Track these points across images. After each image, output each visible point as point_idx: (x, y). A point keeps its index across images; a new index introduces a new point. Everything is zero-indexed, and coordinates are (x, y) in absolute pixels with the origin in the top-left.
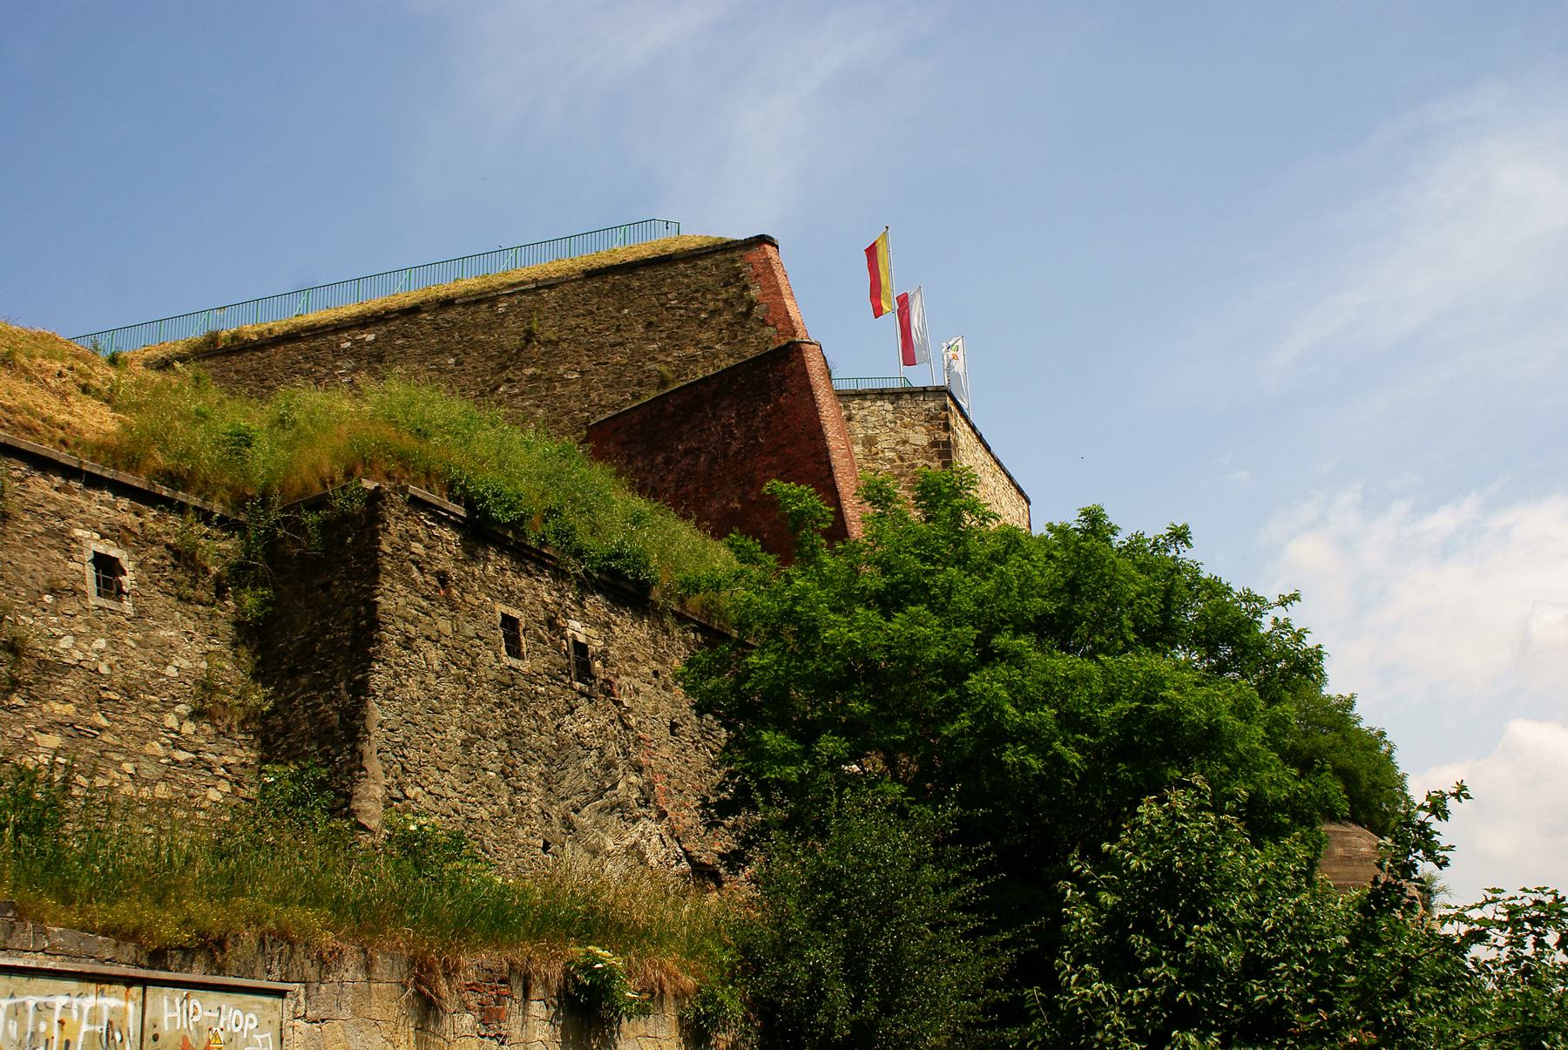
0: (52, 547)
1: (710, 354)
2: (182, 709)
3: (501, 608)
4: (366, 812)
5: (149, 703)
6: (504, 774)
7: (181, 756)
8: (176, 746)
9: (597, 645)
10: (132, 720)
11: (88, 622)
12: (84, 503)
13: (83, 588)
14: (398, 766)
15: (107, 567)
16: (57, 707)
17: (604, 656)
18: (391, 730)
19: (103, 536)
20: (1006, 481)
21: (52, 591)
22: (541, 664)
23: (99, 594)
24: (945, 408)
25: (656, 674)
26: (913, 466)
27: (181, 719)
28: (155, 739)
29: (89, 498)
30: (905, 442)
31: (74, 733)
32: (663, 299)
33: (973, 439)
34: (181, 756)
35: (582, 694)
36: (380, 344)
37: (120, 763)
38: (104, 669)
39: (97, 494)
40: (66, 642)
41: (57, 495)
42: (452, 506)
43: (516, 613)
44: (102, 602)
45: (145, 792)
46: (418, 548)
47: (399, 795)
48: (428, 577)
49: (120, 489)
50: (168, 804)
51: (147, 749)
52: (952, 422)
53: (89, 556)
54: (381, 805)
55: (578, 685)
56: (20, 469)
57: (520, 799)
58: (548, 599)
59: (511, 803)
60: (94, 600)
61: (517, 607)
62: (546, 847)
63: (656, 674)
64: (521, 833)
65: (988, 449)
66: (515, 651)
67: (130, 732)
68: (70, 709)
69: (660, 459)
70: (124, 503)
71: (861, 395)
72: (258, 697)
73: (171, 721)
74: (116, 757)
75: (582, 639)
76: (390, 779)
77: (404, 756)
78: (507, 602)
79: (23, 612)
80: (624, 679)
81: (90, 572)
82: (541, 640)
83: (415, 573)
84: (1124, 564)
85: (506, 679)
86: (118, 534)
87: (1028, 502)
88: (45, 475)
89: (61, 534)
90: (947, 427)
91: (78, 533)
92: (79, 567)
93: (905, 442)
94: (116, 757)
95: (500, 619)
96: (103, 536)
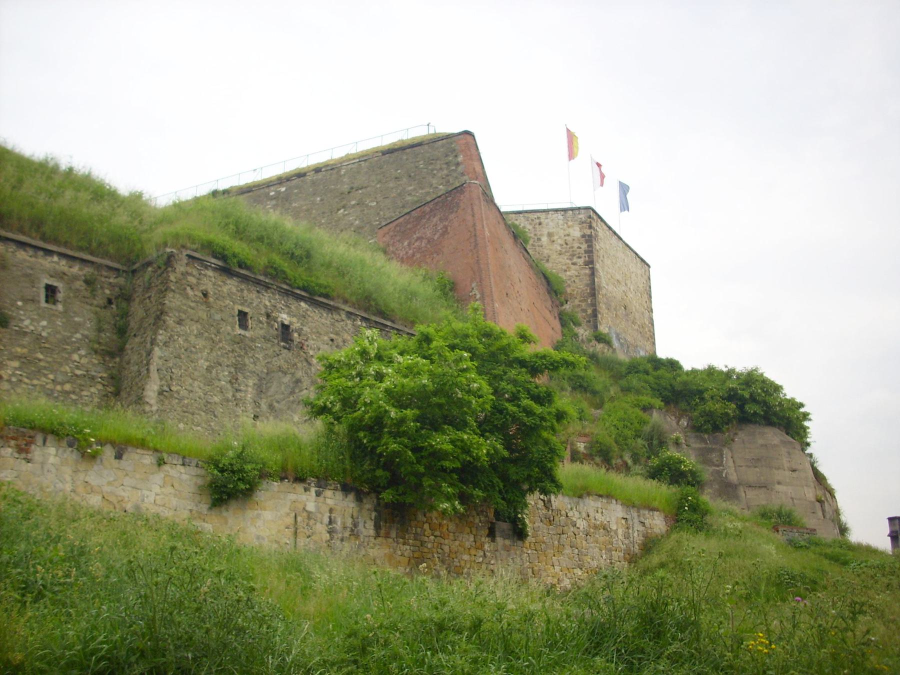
7: (79, 372)
8: (78, 368)
9: (296, 325)
15: (51, 291)
16: (19, 350)
17: (300, 332)
24: (590, 217)
25: (332, 340)
27: (81, 357)
30: (568, 235)
32: (417, 164)
33: (608, 233)
35: (285, 348)
40: (27, 322)
42: (213, 260)
43: (246, 310)
44: (46, 305)
45: (59, 388)
46: (193, 280)
47: (167, 389)
51: (62, 369)
52: (594, 225)
53: (43, 285)
54: (156, 394)
55: (282, 344)
56: (12, 247)
59: (233, 396)
60: (43, 304)
65: (621, 239)
68: (25, 351)
69: (406, 243)
74: (46, 372)
75: (286, 323)
76: (163, 382)
78: (242, 304)
80: (311, 342)
82: (261, 322)
88: (25, 250)
90: (590, 227)
93: (568, 235)
94: (46, 372)
95: (237, 313)
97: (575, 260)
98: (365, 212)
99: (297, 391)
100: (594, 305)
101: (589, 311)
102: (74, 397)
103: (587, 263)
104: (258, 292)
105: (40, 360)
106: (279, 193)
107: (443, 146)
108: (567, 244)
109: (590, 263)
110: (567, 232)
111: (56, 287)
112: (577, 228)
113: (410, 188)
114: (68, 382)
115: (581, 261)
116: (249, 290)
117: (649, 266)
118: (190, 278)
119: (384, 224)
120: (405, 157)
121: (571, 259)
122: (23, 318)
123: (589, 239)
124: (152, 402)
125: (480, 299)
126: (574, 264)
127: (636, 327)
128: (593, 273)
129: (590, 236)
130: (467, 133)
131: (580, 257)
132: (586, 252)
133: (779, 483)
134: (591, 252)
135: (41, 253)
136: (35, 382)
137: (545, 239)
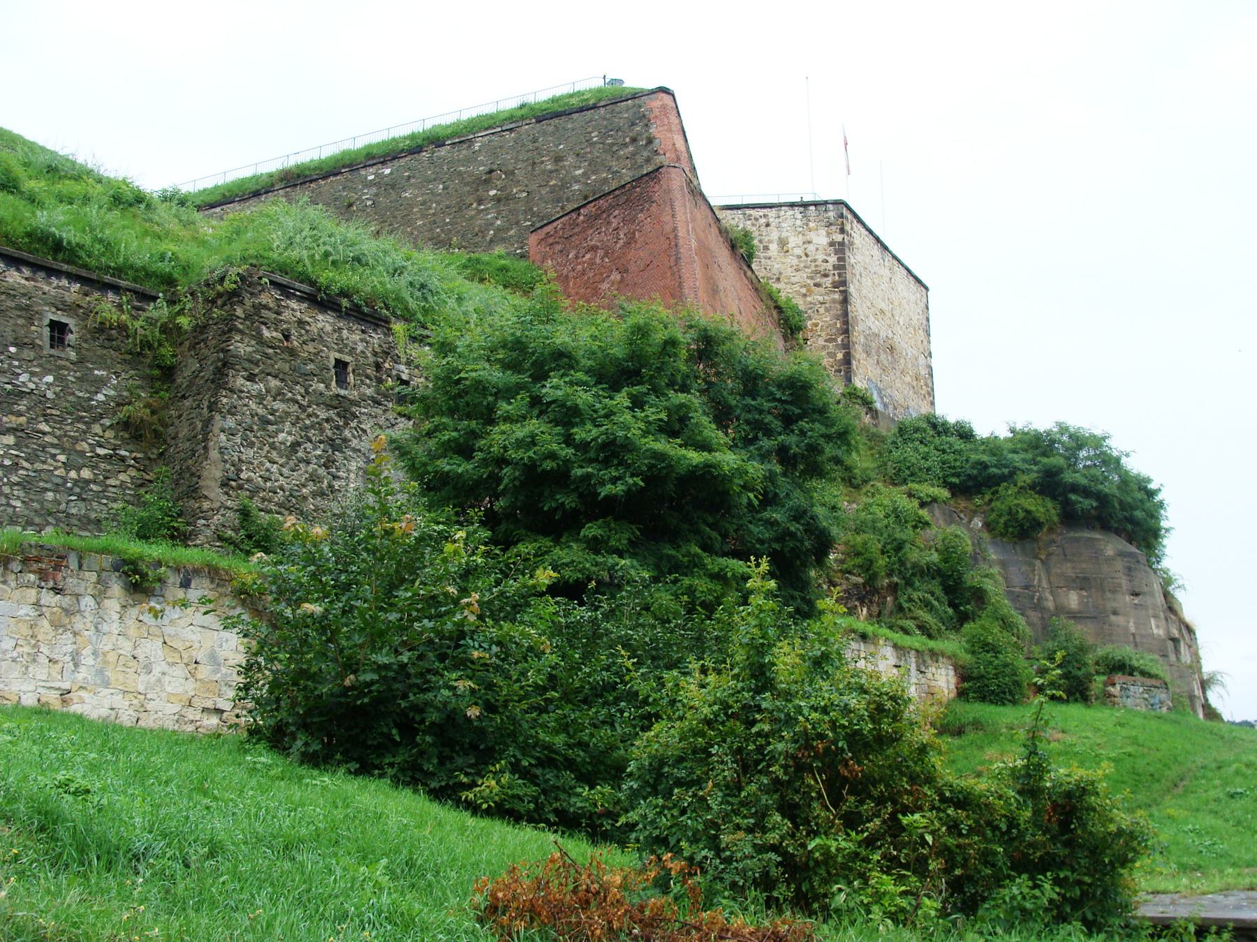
0: (20, 316)
4: (208, 487)
5: (82, 417)
7: (101, 451)
11: (40, 365)
12: (46, 288)
15: (58, 330)
20: (905, 272)
21: (16, 345)
23: (52, 346)
24: (842, 216)
29: (50, 284)
34: (101, 451)
38: (50, 395)
40: (24, 378)
43: (347, 359)
44: (53, 352)
50: (88, 482)
52: (848, 227)
53: (47, 322)
60: (47, 350)
66: (342, 382)
71: (903, 265)
72: (539, 469)
74: (53, 451)
78: (340, 351)
81: (46, 332)
87: (927, 289)
88: (19, 270)
90: (842, 231)
94: (53, 451)
100: (847, 347)
101: (840, 356)
103: (835, 285)
105: (44, 433)
106: (382, 176)
108: (807, 255)
109: (841, 285)
112: (823, 232)
115: (828, 282)
116: (350, 329)
118: (265, 313)
121: (812, 278)
126: (817, 285)
128: (845, 301)
129: (842, 244)
132: (835, 267)
133: (1115, 613)
134: (843, 267)
135: (41, 275)
136: (38, 466)
137: (774, 247)
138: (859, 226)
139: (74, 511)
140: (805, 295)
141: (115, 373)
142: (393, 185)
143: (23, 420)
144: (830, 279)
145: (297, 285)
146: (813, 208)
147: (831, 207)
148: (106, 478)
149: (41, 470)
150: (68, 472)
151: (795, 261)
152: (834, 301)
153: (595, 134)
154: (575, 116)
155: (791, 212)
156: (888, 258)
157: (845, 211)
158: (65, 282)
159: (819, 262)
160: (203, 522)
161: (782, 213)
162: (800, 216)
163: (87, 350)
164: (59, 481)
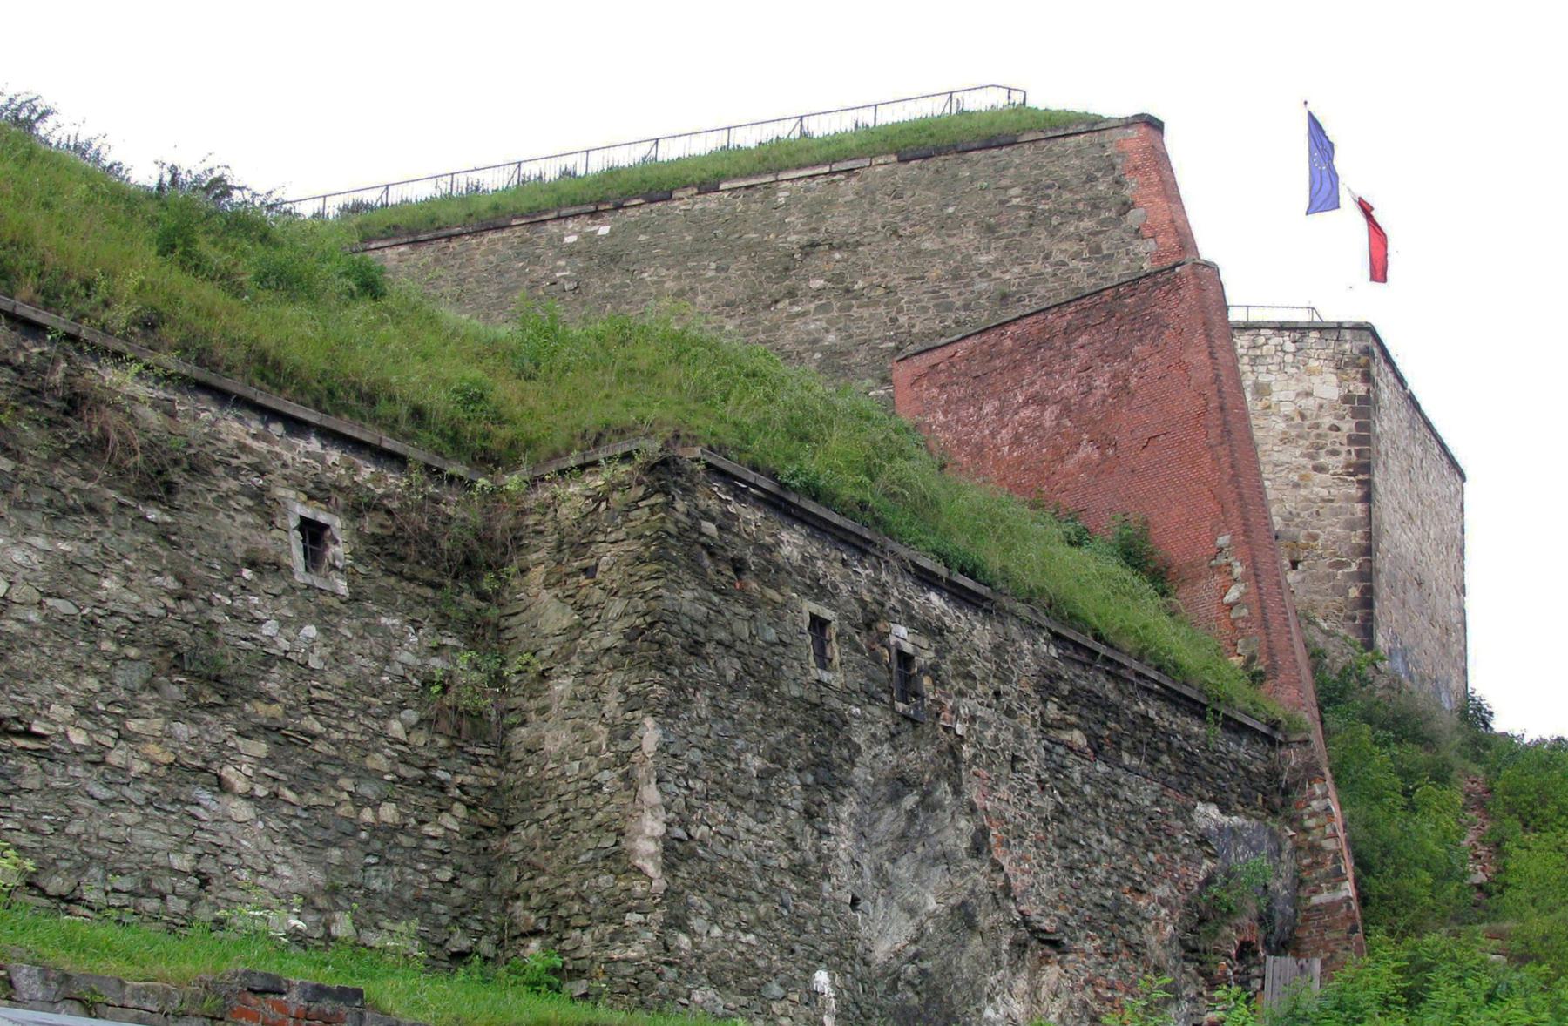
1: (1065, 263)
2: (411, 716)
3: (810, 607)
6: (809, 815)
9: (926, 657)
10: (350, 726)
13: (289, 562)
14: (681, 800)
15: (313, 533)
16: (261, 707)
18: (675, 756)
19: (310, 497)
20: (1437, 450)
21: (252, 564)
22: (856, 680)
23: (307, 570)
26: (1317, 426)
28: (377, 750)
29: (292, 448)
30: (1308, 394)
31: (281, 740)
36: (616, 241)
37: (335, 778)
38: (314, 663)
39: (302, 443)
40: (270, 628)
41: (255, 444)
43: (827, 614)
44: (308, 579)
45: (367, 815)
48: (722, 567)
49: (331, 436)
50: (393, 830)
52: (1374, 371)
53: (294, 522)
55: (900, 706)
57: (826, 843)
58: (867, 598)
60: (301, 576)
61: (830, 606)
62: (855, 902)
63: (997, 694)
64: (826, 886)
66: (824, 662)
67: (347, 741)
70: (334, 455)
73: (396, 728)
74: (332, 771)
75: (908, 648)
76: (671, 815)
77: (688, 788)
78: (817, 599)
79: (218, 589)
82: (858, 649)
83: (707, 561)
84: (71, 154)
85: (814, 698)
86: (319, 492)
89: (259, 495)
90: (1367, 378)
91: (280, 492)
92: (282, 535)
94: (332, 771)
96: (310, 497)
97: (1324, 459)
98: (855, 312)
99: (932, 830)
101: (1354, 592)
102: (405, 840)
104: (844, 563)
105: (314, 737)
106: (591, 238)
107: (1079, 151)
108: (1303, 417)
109: (1362, 469)
110: (1304, 386)
111: (325, 527)
113: (984, 258)
114: (388, 799)
116: (825, 558)
117: (1464, 479)
119: (910, 349)
120: (965, 173)
121: (1311, 457)
122: (259, 615)
123: (1363, 408)
124: (651, 868)
125: (1245, 577)
126: (1319, 469)
127: (1437, 631)
129: (1365, 400)
130: (1154, 125)
131: (1334, 453)
132: (1351, 440)
135: (277, 429)
136: (314, 800)
138: (1387, 369)
139: (376, 884)
140: (1296, 486)
141: (413, 622)
142: (610, 258)
143: (277, 710)
144: (1342, 458)
145: (752, 476)
146: (1314, 335)
147: (1347, 335)
148: (422, 822)
149: (314, 807)
150: (359, 809)
151: (1281, 426)
152: (1348, 498)
153: (1015, 191)
154: (974, 155)
155: (1276, 340)
156: (1420, 425)
157: (1371, 342)
158: (315, 445)
159: (1323, 430)
160: (638, 917)
161: (1261, 340)
162: (1290, 347)
163: (365, 577)
164: (347, 827)
